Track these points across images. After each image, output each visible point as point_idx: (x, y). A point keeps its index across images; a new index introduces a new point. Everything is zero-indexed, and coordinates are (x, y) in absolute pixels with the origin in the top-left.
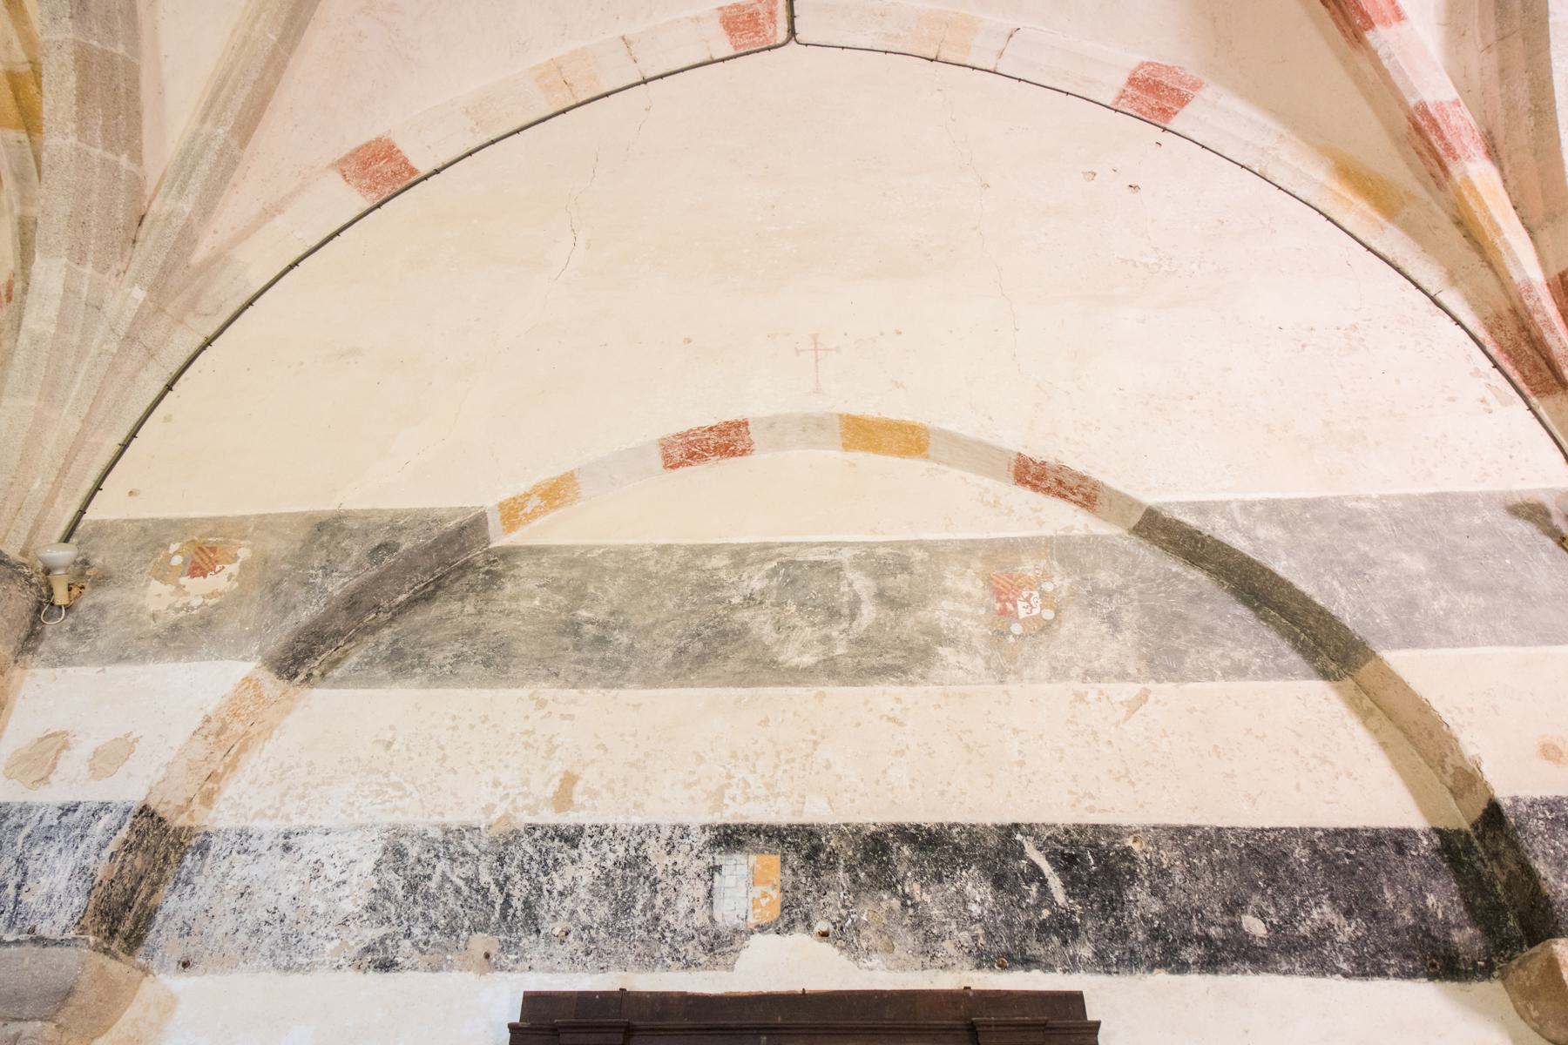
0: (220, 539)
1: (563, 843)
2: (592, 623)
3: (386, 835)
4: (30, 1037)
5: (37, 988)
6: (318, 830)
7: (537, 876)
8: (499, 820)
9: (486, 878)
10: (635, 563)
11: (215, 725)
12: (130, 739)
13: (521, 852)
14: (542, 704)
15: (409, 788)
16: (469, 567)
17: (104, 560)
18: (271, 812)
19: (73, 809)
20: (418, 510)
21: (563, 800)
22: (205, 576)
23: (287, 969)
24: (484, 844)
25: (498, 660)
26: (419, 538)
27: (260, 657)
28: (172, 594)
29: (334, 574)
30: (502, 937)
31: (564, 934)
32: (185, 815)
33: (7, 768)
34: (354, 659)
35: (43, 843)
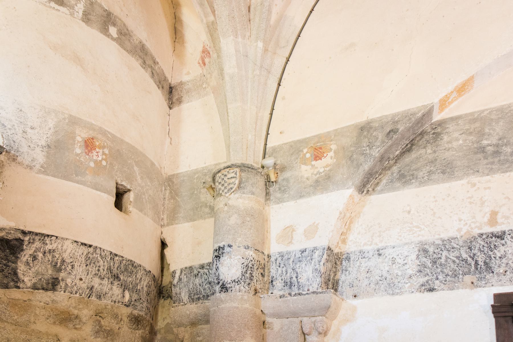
0: (322, 143)
1: (497, 239)
2: (491, 146)
3: (418, 245)
4: (320, 321)
5: (318, 306)
6: (390, 247)
7: (488, 252)
8: (465, 233)
9: (465, 256)
10: (507, 113)
11: (342, 215)
12: (315, 225)
13: (478, 244)
14: (474, 185)
15: (423, 227)
16: (424, 133)
17: (281, 161)
18: (369, 243)
19: (305, 250)
20: (403, 111)
21: (493, 220)
22: (321, 159)
23: (393, 294)
24: (461, 243)
25: (448, 170)
26: (406, 124)
27: (353, 187)
28: (311, 169)
29: (374, 147)
30: (477, 276)
31: (504, 272)
32: (338, 248)
33: (277, 241)
34: (384, 181)
35: (299, 263)
